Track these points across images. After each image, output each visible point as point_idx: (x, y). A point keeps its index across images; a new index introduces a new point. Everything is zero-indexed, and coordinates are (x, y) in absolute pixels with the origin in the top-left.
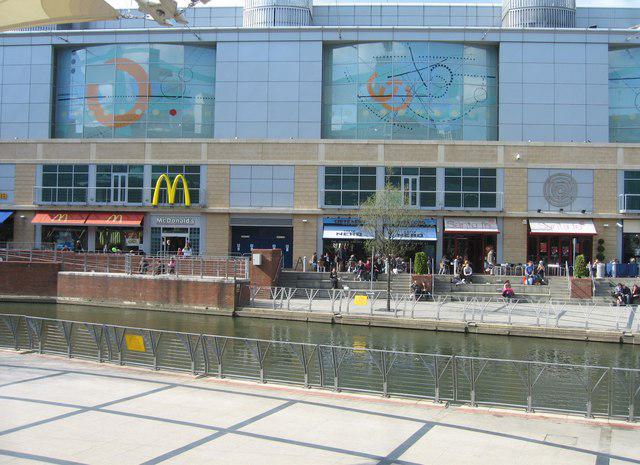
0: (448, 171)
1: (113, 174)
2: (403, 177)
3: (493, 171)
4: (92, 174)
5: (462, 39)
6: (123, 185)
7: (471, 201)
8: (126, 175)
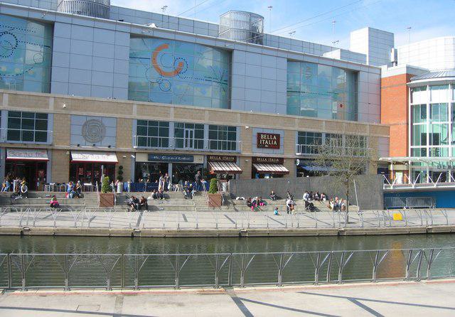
2: (185, 129)
5: (349, 65)
8: (193, 130)
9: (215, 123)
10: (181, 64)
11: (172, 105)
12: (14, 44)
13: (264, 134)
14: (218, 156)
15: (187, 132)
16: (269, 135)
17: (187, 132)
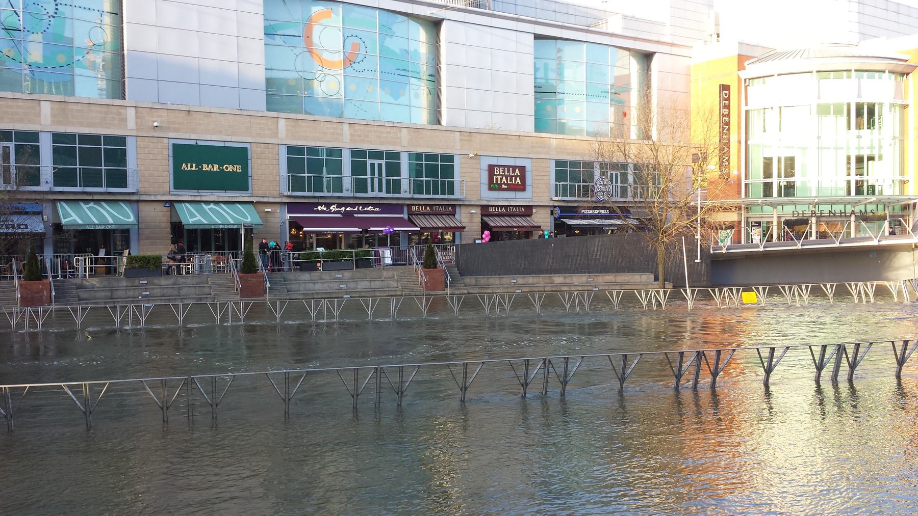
0: (57, 137)
1: (369, 162)
2: (369, 162)
3: (122, 140)
5: (613, 38)
7: (92, 179)
8: (383, 162)
13: (499, 166)
15: (373, 165)
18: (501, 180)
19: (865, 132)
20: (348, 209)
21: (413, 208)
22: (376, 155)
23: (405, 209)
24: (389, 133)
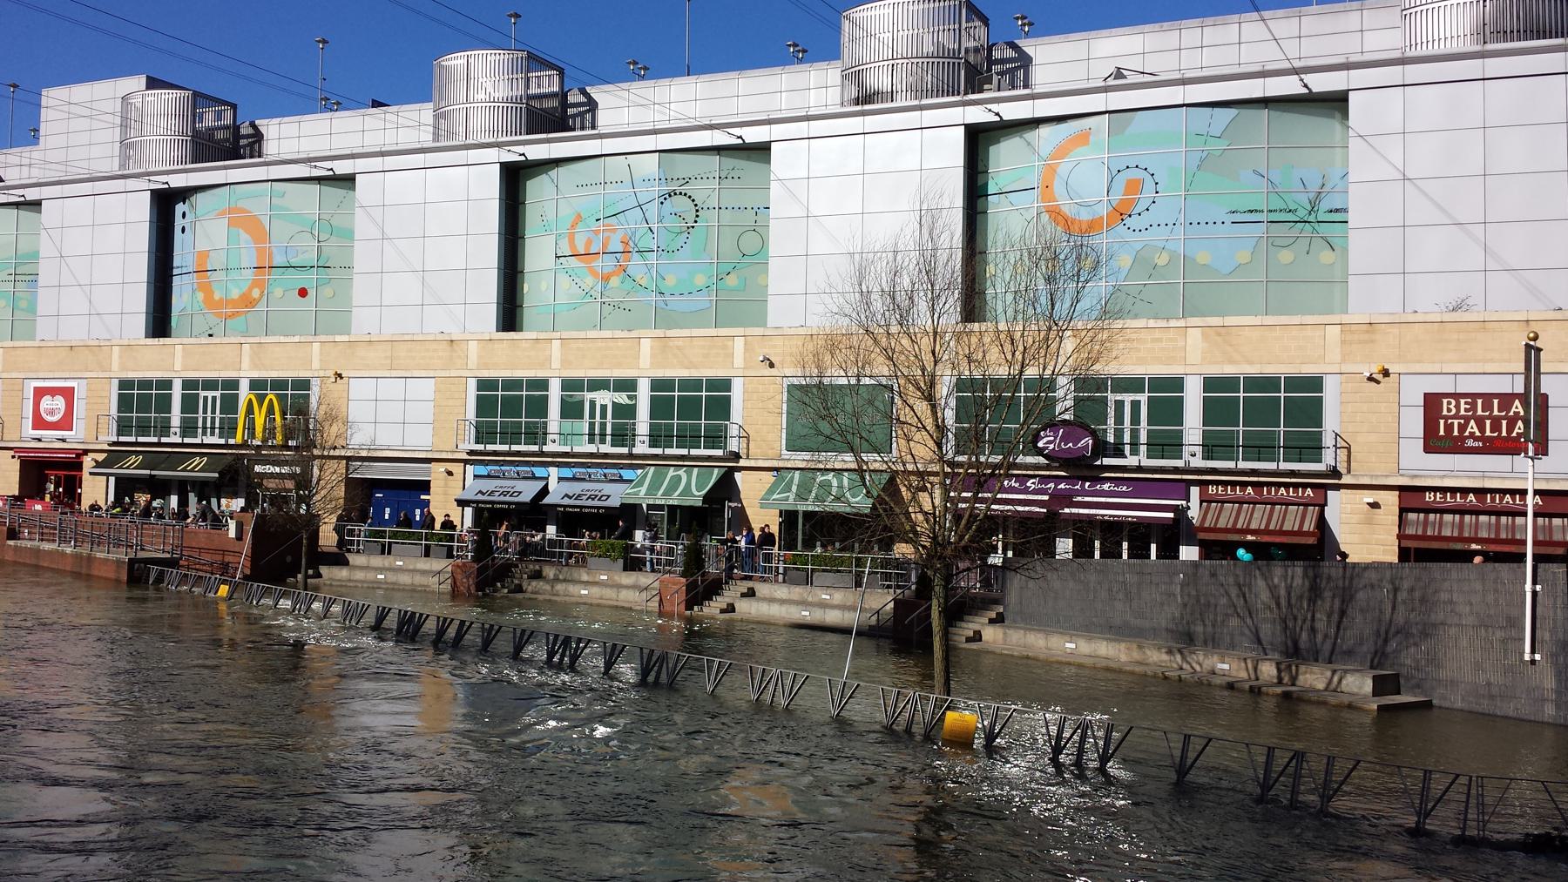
1: (1112, 397)
2: (1112, 397)
4: (177, 393)
6: (1135, 419)
8: (1143, 398)
9: (1228, 370)
10: (1134, 187)
11: (558, 335)
12: (691, 217)
13: (1457, 396)
14: (1465, 491)
15: (206, 398)
16: (1487, 398)
17: (1120, 405)
18: (1462, 428)
19: (1351, 217)
20: (1062, 486)
21: (1212, 490)
22: (210, 385)
23: (1195, 492)
24: (1159, 340)
